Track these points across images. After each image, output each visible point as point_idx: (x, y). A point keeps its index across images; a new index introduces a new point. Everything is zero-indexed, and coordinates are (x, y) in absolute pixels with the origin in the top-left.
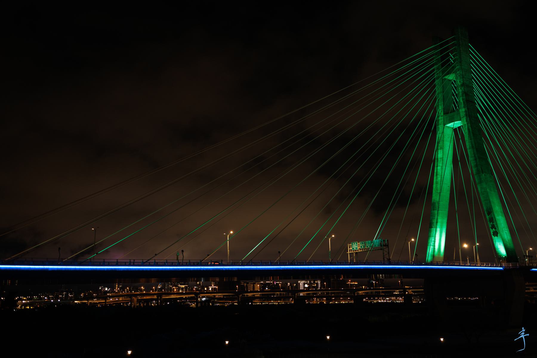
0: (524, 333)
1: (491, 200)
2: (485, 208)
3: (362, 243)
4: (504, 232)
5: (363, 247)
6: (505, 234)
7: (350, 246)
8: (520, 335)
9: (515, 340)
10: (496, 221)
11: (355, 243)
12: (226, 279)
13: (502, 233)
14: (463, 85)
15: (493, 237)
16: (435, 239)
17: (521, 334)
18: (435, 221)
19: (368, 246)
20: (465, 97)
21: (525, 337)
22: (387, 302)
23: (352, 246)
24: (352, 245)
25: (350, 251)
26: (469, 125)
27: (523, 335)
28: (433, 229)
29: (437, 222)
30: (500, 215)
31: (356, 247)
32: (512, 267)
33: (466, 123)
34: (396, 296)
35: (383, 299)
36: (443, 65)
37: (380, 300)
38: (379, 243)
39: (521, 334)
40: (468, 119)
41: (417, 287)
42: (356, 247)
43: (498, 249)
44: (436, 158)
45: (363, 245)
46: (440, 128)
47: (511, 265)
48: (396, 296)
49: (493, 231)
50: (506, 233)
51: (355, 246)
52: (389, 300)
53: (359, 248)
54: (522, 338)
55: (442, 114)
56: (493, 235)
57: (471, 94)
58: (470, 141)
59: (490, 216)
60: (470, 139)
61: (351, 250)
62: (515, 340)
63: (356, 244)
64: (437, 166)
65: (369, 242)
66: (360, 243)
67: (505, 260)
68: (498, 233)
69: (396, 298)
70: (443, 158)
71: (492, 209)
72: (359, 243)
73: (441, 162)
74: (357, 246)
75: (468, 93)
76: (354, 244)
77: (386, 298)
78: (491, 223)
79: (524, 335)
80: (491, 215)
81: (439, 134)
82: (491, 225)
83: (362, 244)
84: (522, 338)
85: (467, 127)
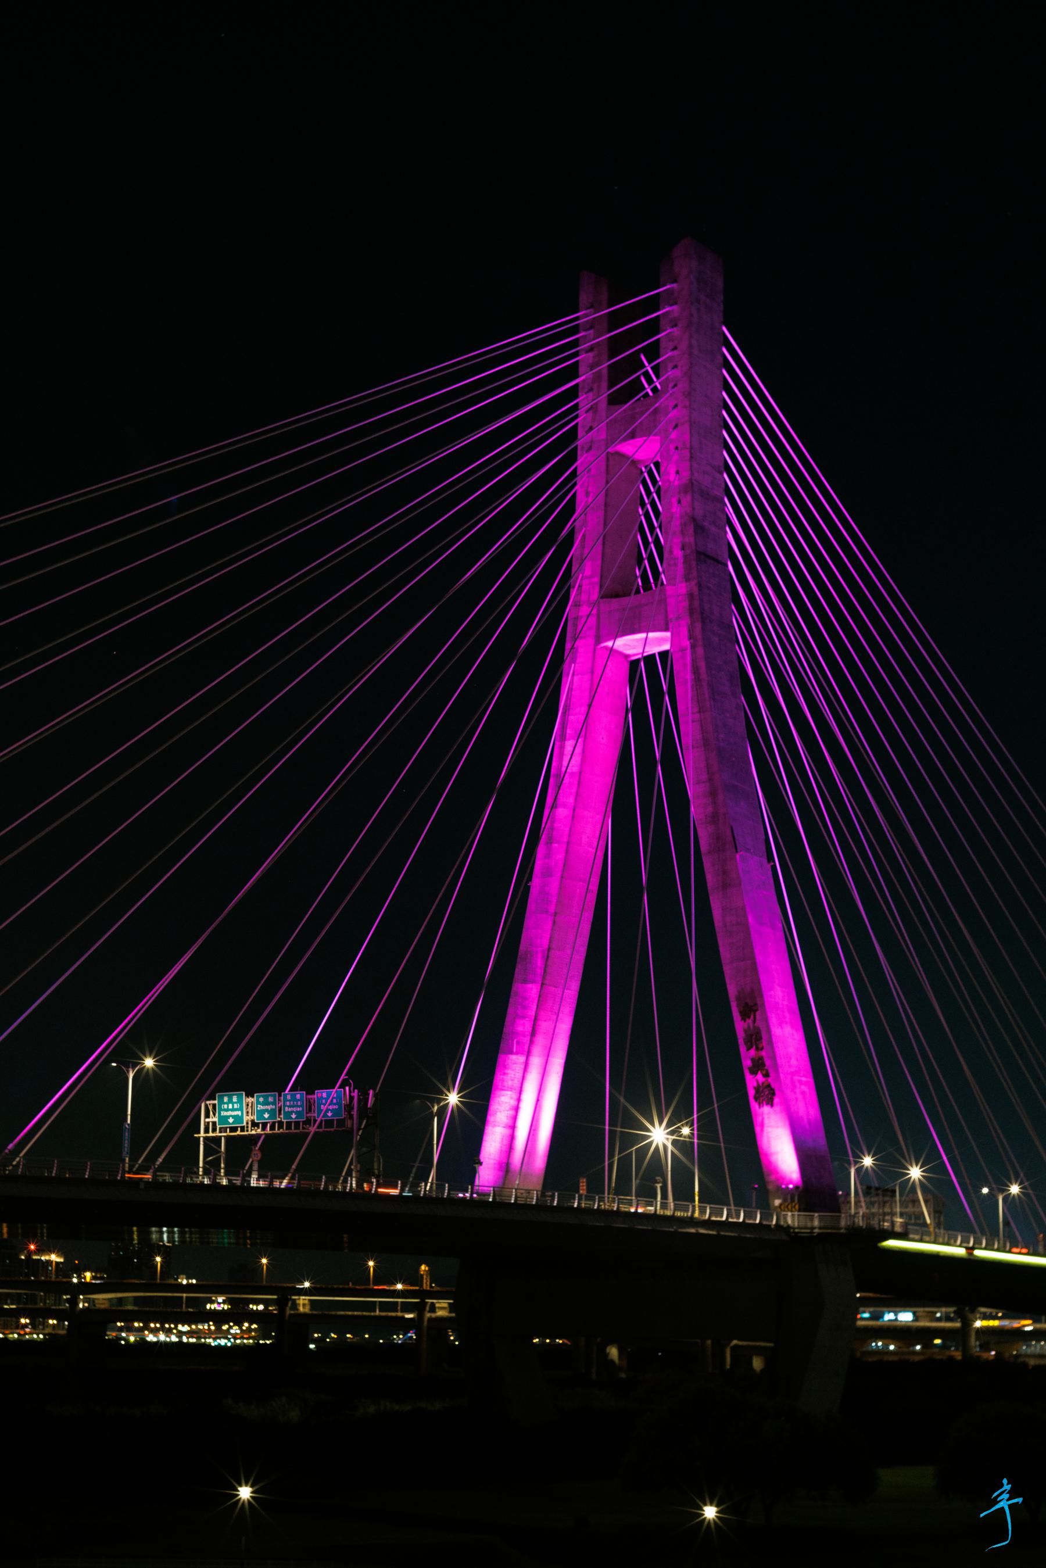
0: (1008, 1496)
1: (759, 959)
2: (732, 991)
3: (266, 1098)
4: (798, 1091)
5: (294, 1116)
6: (800, 1096)
7: (211, 1108)
8: (996, 1502)
9: (982, 1515)
10: (771, 1042)
11: (235, 1099)
12: (171, 1233)
13: (788, 1093)
14: (690, 487)
15: (754, 1105)
16: (519, 1100)
17: (998, 1499)
18: (524, 1026)
19: (292, 1112)
20: (692, 540)
21: (1010, 1506)
22: (180, 1342)
23: (220, 1110)
24: (221, 1102)
25: (207, 1131)
26: (700, 651)
27: (1005, 1501)
28: (514, 1057)
29: (533, 1033)
30: (786, 1023)
31: (239, 1113)
32: (820, 1228)
33: (688, 643)
34: (219, 1318)
35: (163, 1329)
36: (615, 400)
37: (155, 1331)
38: (339, 1103)
39: (998, 1499)
40: (698, 626)
41: (335, 1286)
42: (239, 1113)
43: (771, 1154)
44: (553, 771)
45: (269, 1107)
46: (581, 650)
47: (816, 1223)
48: (219, 1318)
49: (755, 1085)
50: (803, 1093)
51: (233, 1110)
52: (190, 1334)
53: (250, 1118)
54: (1002, 1509)
55: (595, 596)
56: (756, 1099)
57: (713, 528)
58: (698, 715)
59: (750, 1021)
60: (697, 709)
61: (214, 1123)
62: (982, 1515)
63: (240, 1101)
64: (554, 806)
65: (298, 1096)
66: (254, 1100)
67: (792, 1200)
68: (774, 1094)
69: (219, 1329)
70: (580, 772)
71: (762, 996)
72: (250, 1100)
73: (574, 791)
74: (241, 1109)
75: (706, 524)
76: (230, 1101)
77: (176, 1328)
78: (753, 1052)
79: (1007, 1500)
80: (754, 1021)
81: (573, 675)
82: (753, 1060)
83: (265, 1103)
84: (1002, 1509)
85: (689, 659)
